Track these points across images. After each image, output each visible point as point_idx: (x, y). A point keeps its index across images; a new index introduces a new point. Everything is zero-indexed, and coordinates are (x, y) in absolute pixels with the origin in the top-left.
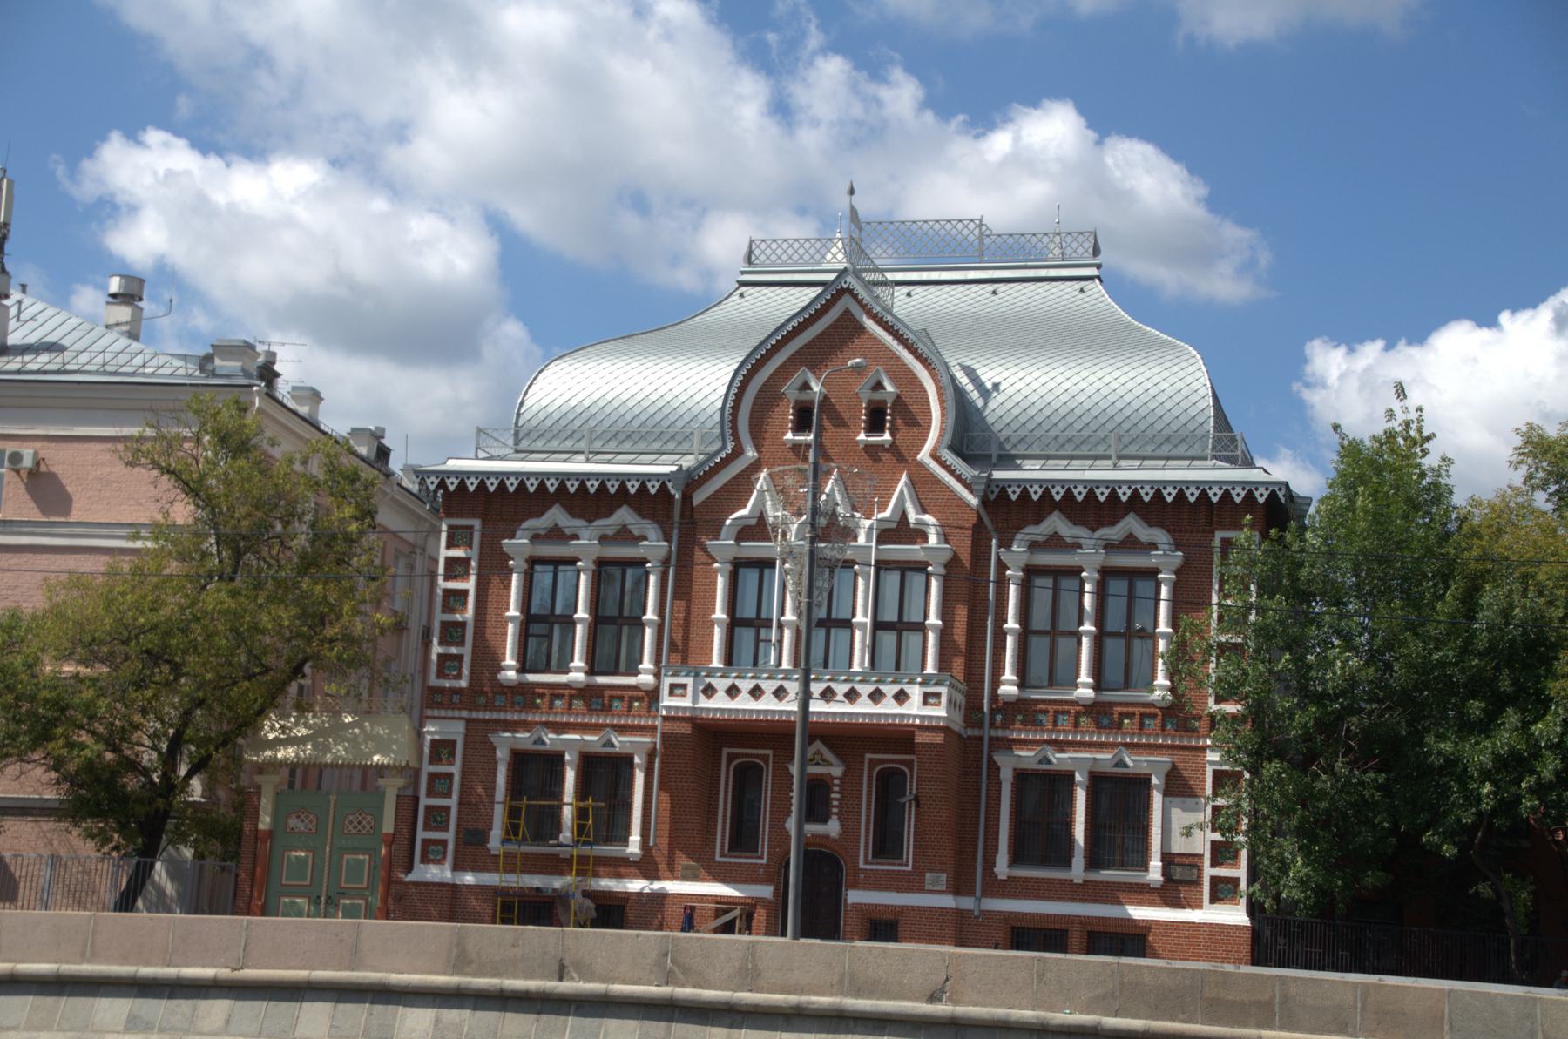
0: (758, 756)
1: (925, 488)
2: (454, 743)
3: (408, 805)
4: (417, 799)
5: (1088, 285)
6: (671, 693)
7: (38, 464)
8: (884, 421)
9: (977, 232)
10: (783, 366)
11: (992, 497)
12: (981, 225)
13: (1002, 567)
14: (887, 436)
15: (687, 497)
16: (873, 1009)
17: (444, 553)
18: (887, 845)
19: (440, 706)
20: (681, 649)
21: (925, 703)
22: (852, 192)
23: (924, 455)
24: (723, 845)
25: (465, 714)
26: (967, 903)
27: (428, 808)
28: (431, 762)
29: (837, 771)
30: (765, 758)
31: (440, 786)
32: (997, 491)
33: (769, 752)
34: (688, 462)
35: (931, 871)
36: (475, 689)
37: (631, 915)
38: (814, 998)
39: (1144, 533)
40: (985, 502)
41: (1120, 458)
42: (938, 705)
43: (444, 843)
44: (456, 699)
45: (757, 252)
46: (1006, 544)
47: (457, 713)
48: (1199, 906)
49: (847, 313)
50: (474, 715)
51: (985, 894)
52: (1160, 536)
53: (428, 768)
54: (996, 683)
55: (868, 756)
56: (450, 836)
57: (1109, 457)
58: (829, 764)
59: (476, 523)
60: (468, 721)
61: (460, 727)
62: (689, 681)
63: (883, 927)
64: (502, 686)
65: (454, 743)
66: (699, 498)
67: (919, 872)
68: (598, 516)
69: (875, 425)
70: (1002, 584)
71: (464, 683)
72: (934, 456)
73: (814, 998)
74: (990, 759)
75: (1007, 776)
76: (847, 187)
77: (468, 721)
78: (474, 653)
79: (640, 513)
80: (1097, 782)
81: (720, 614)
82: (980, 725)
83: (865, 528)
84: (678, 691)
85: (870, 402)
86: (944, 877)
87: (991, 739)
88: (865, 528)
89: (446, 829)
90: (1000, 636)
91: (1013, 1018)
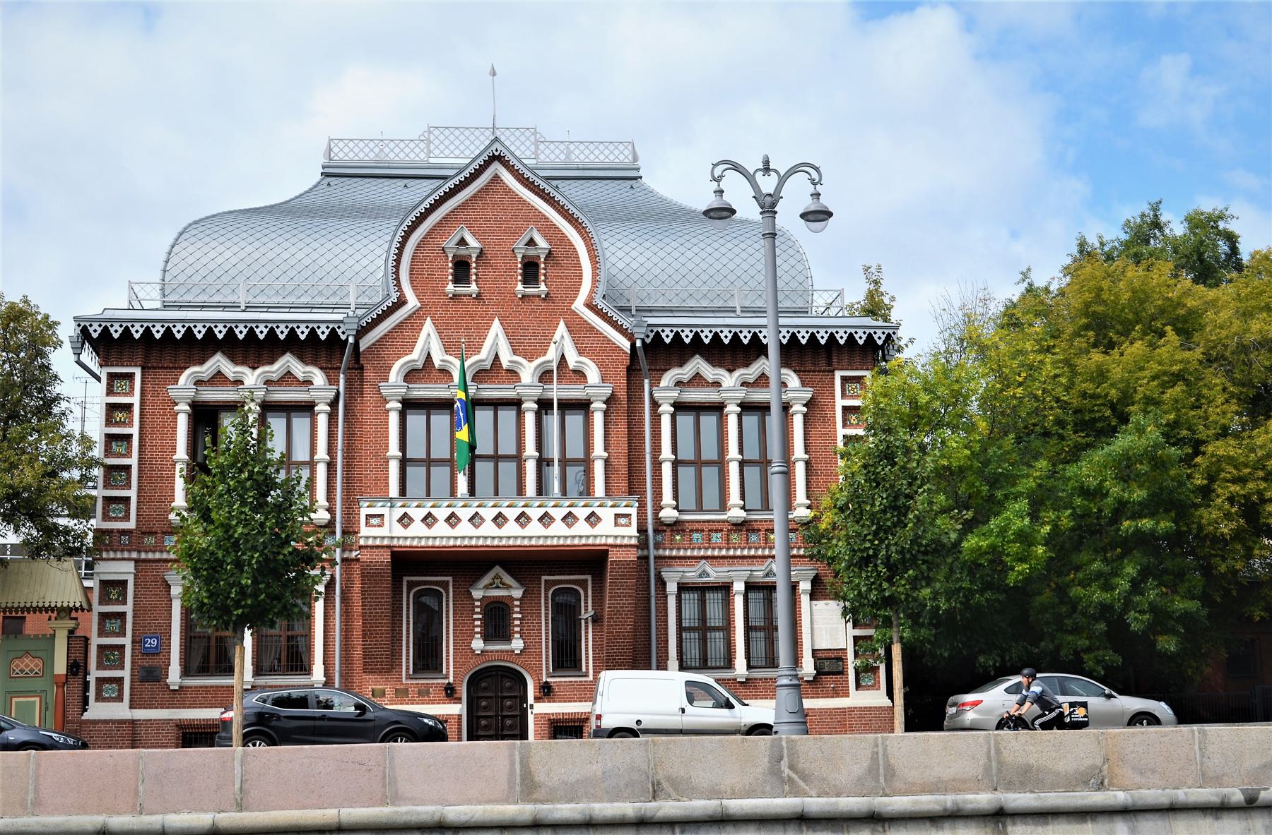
0: (437, 583)
1: (580, 331)
2: (124, 583)
3: (78, 643)
4: (86, 639)
6: (367, 524)
10: (439, 224)
12: (535, 133)
13: (655, 405)
14: (543, 287)
15: (356, 344)
16: (827, 808)
18: (567, 657)
19: (110, 548)
21: (616, 524)
22: (494, 74)
23: (579, 305)
24: (408, 668)
25: (134, 555)
27: (100, 647)
28: (100, 603)
29: (517, 593)
30: (445, 585)
33: (450, 579)
38: (970, 797)
42: (629, 525)
43: (120, 681)
44: (125, 539)
45: (336, 150)
46: (655, 382)
47: (126, 555)
48: (847, 695)
49: (496, 178)
50: (143, 556)
53: (98, 608)
55: (544, 578)
58: (509, 587)
59: (138, 372)
60: (137, 561)
61: (130, 567)
62: (385, 511)
64: (663, 524)
65: (124, 583)
66: (364, 344)
70: (656, 417)
71: (131, 524)
72: (590, 306)
73: (419, 808)
75: (672, 588)
76: (489, 68)
77: (137, 561)
78: (139, 496)
81: (394, 449)
83: (528, 372)
84: (374, 521)
88: (528, 372)
90: (657, 465)
91: (402, 814)
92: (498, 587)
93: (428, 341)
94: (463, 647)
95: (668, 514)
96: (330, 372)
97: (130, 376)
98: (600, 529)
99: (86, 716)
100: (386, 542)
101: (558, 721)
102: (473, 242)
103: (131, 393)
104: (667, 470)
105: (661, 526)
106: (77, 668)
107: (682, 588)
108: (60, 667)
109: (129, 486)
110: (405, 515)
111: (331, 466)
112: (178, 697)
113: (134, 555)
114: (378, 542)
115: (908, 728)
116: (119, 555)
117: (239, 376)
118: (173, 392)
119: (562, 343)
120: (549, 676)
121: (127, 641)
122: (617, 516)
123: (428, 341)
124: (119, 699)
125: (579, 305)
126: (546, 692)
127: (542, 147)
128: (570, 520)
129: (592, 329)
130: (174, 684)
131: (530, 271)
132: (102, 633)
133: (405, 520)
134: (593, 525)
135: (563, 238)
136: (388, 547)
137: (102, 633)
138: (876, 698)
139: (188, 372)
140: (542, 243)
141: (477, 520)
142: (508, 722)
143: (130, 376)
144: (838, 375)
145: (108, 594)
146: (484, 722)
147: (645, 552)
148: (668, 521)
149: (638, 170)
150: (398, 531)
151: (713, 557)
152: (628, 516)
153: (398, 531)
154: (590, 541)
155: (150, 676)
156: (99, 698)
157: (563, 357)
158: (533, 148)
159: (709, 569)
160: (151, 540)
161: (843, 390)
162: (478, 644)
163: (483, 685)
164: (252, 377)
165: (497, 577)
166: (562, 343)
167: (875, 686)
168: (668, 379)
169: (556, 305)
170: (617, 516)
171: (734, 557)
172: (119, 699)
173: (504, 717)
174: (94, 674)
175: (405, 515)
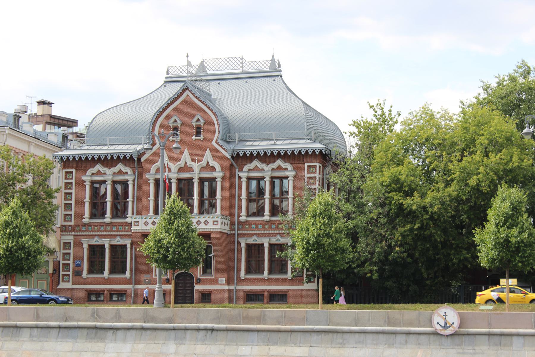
1: (214, 152)
2: (70, 243)
4: (59, 261)
5: (276, 78)
7: (511, 136)
8: (201, 132)
9: (241, 61)
11: (235, 156)
15: (139, 159)
17: (307, 175)
20: (140, 211)
21: (214, 224)
23: (214, 143)
25: (73, 233)
26: (232, 287)
31: (67, 257)
32: (236, 153)
34: (139, 147)
35: (220, 277)
36: (76, 225)
37: (213, 297)
39: (284, 165)
40: (232, 157)
41: (277, 140)
42: (218, 225)
45: (170, 71)
46: (241, 170)
47: (71, 233)
50: (76, 234)
51: (237, 284)
52: (289, 166)
54: (239, 216)
56: (71, 273)
57: (273, 140)
59: (74, 171)
60: (74, 235)
61: (72, 238)
63: (206, 297)
64: (241, 222)
65: (70, 243)
67: (217, 278)
68: (112, 166)
69: (198, 133)
70: (240, 183)
71: (72, 223)
74: (238, 241)
79: (126, 165)
80: (113, 248)
82: (234, 230)
84: (137, 224)
85: (196, 125)
86: (224, 279)
87: (238, 234)
89: (69, 271)
90: (240, 201)
95: (243, 218)
96: (133, 168)
97: (72, 172)
99: (59, 287)
100: (140, 231)
101: (202, 292)
103: (72, 179)
104: (244, 203)
105: (240, 223)
106: (56, 271)
108: (51, 271)
109: (71, 210)
110: (146, 222)
111: (133, 202)
112: (86, 281)
113: (73, 233)
114: (137, 231)
115: (176, 302)
116: (68, 234)
117: (104, 172)
118: (84, 178)
119: (208, 156)
120: (201, 276)
121: (71, 262)
122: (214, 221)
124: (69, 281)
125: (214, 143)
126: (199, 281)
127: (244, 64)
128: (199, 223)
129: (218, 151)
131: (198, 130)
132: (64, 260)
133: (146, 223)
134: (206, 225)
135: (210, 117)
136: (140, 232)
137: (64, 260)
138: (312, 286)
139: (89, 170)
142: (188, 291)
143: (72, 172)
144: (306, 164)
145: (66, 246)
146: (180, 291)
147: (234, 232)
148: (243, 221)
149: (280, 71)
150: (144, 227)
151: (258, 234)
152: (217, 221)
153: (144, 227)
154: (205, 230)
155: (78, 273)
156: (63, 281)
157: (208, 162)
158: (241, 65)
159: (256, 239)
160: (78, 228)
161: (308, 170)
163: (181, 278)
164: (109, 172)
166: (208, 156)
167: (314, 282)
168: (246, 168)
169: (206, 144)
170: (214, 221)
171: (266, 234)
172: (69, 281)
173: (186, 290)
174: (62, 273)
175: (146, 222)
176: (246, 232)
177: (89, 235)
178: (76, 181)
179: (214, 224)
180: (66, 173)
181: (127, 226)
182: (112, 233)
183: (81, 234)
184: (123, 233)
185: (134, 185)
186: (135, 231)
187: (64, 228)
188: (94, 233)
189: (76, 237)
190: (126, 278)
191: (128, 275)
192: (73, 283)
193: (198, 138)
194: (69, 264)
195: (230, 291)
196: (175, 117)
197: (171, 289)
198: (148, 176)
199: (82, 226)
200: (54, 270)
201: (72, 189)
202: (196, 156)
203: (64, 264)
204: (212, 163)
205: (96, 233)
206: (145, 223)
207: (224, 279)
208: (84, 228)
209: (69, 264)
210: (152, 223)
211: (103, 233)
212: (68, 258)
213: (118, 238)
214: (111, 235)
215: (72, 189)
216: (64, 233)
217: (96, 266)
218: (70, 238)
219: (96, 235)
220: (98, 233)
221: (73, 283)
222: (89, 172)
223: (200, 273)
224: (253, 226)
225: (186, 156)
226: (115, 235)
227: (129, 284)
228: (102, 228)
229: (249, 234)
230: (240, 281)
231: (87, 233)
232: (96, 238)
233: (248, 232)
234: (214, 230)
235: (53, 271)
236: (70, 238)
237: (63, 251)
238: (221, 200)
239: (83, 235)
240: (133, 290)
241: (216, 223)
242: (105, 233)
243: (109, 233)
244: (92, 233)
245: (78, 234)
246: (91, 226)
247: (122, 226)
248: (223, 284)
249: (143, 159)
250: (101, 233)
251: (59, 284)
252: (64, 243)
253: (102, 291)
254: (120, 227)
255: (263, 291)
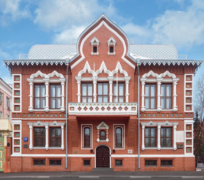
2: (19, 125)
15: (70, 68)
21: (132, 110)
23: (123, 57)
25: (21, 119)
30: (91, 126)
31: (17, 135)
33: (92, 125)
35: (129, 149)
39: (170, 74)
50: (24, 119)
55: (114, 125)
56: (20, 146)
59: (21, 75)
61: (21, 121)
65: (19, 125)
67: (126, 150)
71: (21, 111)
74: (140, 124)
84: (72, 109)
86: (132, 150)
92: (103, 127)
93: (87, 66)
94: (95, 141)
97: (19, 76)
98: (128, 111)
100: (75, 114)
102: (97, 41)
103: (19, 137)
107: (146, 127)
108: (5, 144)
109: (19, 103)
110: (80, 107)
111: (65, 98)
112: (32, 152)
113: (21, 119)
114: (73, 114)
119: (119, 67)
120: (114, 148)
122: (132, 108)
123: (87, 66)
124: (19, 152)
125: (123, 57)
126: (114, 152)
130: (143, 149)
136: (75, 115)
137: (15, 136)
140: (114, 41)
141: (97, 109)
143: (19, 76)
145: (16, 128)
152: (135, 108)
155: (26, 147)
156: (15, 151)
160: (25, 115)
162: (98, 140)
164: (47, 76)
165: (103, 124)
166: (119, 67)
169: (118, 58)
172: (19, 152)
174: (13, 146)
175: (80, 107)
176: (144, 119)
177: (33, 120)
178: (22, 89)
179: (132, 110)
180: (15, 76)
181: (61, 114)
182: (50, 119)
183: (27, 119)
184: (58, 119)
185: (65, 86)
186: (71, 114)
187: (15, 115)
188: (37, 119)
189: (23, 121)
190: (61, 150)
191: (62, 147)
192: (22, 153)
193: (112, 54)
194: (19, 140)
195: (137, 159)
196: (95, 39)
197: (94, 157)
198: (76, 78)
199: (28, 114)
200: (8, 144)
201: (19, 88)
202: (111, 67)
203: (15, 140)
204: (122, 71)
205: (38, 119)
206: (78, 109)
207: (132, 150)
208: (29, 115)
209: (19, 140)
210: (84, 108)
211: (43, 119)
212: (18, 135)
213: (55, 122)
214: (50, 120)
215: (19, 88)
216: (15, 119)
217: (39, 140)
218: (19, 122)
219: (38, 120)
220: (40, 119)
221: (22, 153)
222: (32, 76)
223: (114, 147)
224: (153, 115)
225: (103, 66)
226: (52, 120)
227: (64, 154)
228: (43, 115)
229: (147, 120)
230: (142, 152)
231: (32, 119)
232: (39, 122)
233: (146, 119)
234: (133, 114)
235: (7, 144)
236: (19, 122)
237: (14, 131)
238: (129, 96)
239: (29, 120)
240: (66, 158)
241: (134, 109)
242: (45, 119)
243: (48, 119)
244: (35, 119)
245: (25, 119)
246: (34, 114)
247: (57, 114)
248: (131, 154)
249: (72, 67)
250: (41, 119)
251: (12, 153)
252: (15, 125)
253: (43, 158)
254: (56, 115)
255: (157, 158)
